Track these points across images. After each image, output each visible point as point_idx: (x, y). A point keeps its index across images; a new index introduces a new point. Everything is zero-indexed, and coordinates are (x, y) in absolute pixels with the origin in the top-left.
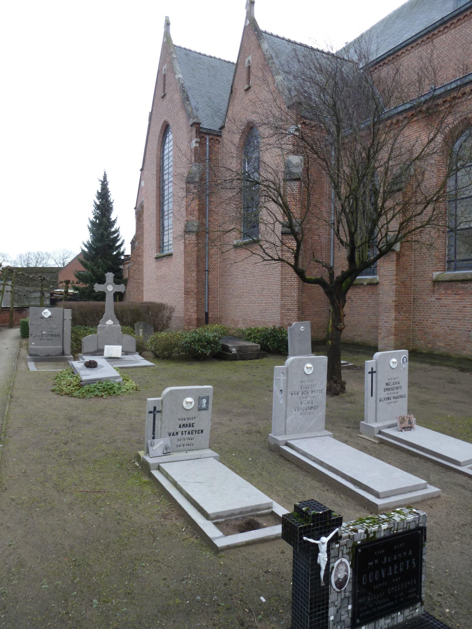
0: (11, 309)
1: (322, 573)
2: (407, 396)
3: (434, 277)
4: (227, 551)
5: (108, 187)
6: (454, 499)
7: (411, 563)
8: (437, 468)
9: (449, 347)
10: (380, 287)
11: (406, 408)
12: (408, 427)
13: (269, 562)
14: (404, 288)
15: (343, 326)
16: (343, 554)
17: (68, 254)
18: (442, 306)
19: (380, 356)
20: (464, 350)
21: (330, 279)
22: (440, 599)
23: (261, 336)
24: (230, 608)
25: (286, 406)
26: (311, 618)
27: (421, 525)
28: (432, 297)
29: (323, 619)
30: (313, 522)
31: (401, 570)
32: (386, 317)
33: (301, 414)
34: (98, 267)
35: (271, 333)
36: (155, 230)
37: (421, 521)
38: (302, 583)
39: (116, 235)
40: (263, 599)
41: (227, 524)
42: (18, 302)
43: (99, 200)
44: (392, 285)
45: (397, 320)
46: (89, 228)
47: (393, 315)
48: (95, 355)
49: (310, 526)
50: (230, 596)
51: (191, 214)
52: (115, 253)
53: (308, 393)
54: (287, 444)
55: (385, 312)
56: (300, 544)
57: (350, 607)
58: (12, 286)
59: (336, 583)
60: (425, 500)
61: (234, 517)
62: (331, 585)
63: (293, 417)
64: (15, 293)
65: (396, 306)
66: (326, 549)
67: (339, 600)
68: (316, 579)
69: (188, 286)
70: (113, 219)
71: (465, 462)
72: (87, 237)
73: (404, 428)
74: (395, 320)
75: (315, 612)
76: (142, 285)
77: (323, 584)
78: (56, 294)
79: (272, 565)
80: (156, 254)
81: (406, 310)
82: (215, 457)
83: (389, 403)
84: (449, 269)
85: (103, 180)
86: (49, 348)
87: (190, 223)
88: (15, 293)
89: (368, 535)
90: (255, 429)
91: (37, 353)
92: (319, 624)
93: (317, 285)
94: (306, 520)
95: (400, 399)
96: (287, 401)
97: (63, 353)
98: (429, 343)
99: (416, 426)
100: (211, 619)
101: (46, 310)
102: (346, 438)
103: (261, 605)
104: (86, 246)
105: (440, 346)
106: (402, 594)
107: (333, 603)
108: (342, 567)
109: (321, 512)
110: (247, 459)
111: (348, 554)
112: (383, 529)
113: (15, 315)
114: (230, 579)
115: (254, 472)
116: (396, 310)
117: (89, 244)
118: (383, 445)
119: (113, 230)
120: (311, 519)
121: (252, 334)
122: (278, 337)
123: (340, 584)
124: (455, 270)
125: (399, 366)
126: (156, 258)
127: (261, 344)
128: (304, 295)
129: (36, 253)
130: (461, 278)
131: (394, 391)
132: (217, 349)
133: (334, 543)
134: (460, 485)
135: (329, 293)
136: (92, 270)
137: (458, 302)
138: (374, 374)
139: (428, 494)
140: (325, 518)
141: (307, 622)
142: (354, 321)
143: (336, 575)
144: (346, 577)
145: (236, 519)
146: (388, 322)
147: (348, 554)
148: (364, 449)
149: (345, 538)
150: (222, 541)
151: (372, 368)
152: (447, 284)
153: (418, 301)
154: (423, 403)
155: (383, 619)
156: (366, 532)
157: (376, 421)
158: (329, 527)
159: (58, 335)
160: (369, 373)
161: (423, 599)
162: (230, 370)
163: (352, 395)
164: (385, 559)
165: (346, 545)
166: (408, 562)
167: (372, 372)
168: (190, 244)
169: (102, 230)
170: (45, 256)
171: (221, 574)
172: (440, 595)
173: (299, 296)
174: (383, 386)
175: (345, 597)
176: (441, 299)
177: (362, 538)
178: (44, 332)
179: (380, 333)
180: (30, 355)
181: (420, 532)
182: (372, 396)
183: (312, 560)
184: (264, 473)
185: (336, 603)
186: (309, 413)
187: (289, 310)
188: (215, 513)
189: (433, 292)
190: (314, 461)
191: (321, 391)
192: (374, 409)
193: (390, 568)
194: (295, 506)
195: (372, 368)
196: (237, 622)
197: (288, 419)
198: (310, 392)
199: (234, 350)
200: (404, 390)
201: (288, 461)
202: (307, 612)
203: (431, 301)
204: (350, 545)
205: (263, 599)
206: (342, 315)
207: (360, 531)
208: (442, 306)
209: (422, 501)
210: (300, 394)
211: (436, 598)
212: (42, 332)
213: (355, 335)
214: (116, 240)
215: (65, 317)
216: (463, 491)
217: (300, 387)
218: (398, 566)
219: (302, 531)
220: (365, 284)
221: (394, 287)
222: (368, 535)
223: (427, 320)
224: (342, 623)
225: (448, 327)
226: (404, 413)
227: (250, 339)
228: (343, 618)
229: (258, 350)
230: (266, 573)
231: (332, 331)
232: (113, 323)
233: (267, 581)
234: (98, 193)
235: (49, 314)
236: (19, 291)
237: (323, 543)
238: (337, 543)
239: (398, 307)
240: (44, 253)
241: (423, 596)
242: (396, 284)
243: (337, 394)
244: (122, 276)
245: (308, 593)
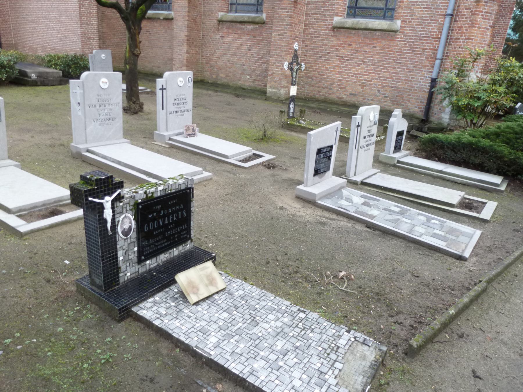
1: (109, 225)
2: (192, 110)
3: (219, 17)
4: (32, 234)
6: (222, 180)
7: (182, 214)
8: (212, 161)
9: (228, 78)
10: (174, 21)
11: (191, 120)
12: (192, 134)
13: (72, 237)
14: (194, 24)
15: (139, 52)
16: (126, 210)
18: (224, 43)
19: (169, 75)
20: (240, 80)
21: (126, 5)
22: (206, 239)
23: (62, 62)
24: (37, 273)
25: (85, 118)
26: (103, 260)
27: (189, 186)
28: (216, 34)
29: (113, 259)
30: (96, 185)
31: (175, 219)
32: (179, 50)
33: (100, 125)
35: (72, 60)
37: (189, 183)
38: (93, 236)
40: (67, 262)
41: (31, 215)
44: (184, 21)
45: (189, 53)
47: (185, 48)
49: (94, 189)
50: (36, 265)
53: (105, 106)
54: (88, 151)
55: (179, 46)
56: (87, 204)
57: (136, 249)
59: (123, 233)
60: (201, 182)
61: (37, 209)
62: (119, 235)
63: (92, 127)
65: (187, 40)
66: (110, 206)
67: (126, 245)
68: (104, 230)
71: (231, 155)
73: (189, 135)
74: (187, 53)
75: (106, 255)
77: (110, 233)
79: (75, 238)
81: (196, 45)
82: (15, 166)
83: (177, 116)
84: (231, 11)
89: (147, 195)
90: (58, 142)
92: (110, 264)
93: (114, 10)
94: (91, 185)
95: (186, 113)
96: (85, 113)
98: (214, 75)
99: (198, 134)
100: (19, 284)
102: (142, 145)
103: (65, 266)
105: (222, 77)
106: (176, 236)
107: (122, 247)
108: (127, 221)
109: (103, 177)
110: (51, 166)
111: (131, 210)
112: (159, 190)
114: (35, 254)
115: (57, 176)
116: (187, 44)
118: (172, 149)
120: (94, 183)
121: (52, 61)
122: (80, 65)
123: (126, 233)
124: (236, 12)
125: (185, 84)
127: (63, 72)
128: (104, 25)
130: (240, 20)
131: (181, 106)
132: (13, 74)
133: (118, 203)
134: (227, 171)
135: (125, 19)
137: (236, 40)
138: (164, 91)
139: (204, 177)
140: (108, 182)
141: (100, 264)
142: (152, 53)
143: (121, 227)
144: (130, 228)
145: (40, 210)
146: (181, 55)
147: (131, 210)
148: (158, 152)
149: (127, 198)
150: (23, 226)
151: (163, 86)
152: (229, 24)
153: (206, 38)
154: (206, 119)
155: (163, 254)
156: (145, 193)
157: (167, 131)
158: (112, 189)
160: (160, 89)
161: (192, 238)
162: (31, 94)
163: (149, 113)
164: (162, 211)
165: (129, 203)
166: (180, 213)
167: (162, 89)
171: (26, 251)
172: (206, 237)
173: (99, 25)
174: (171, 101)
175: (131, 242)
176: (224, 37)
177: (142, 197)
179: (174, 65)
181: (188, 191)
182: (163, 109)
183: (99, 216)
184: (68, 175)
185: (124, 247)
186: (108, 124)
187: (89, 38)
188: (17, 208)
189: (218, 30)
190: (113, 162)
191: (118, 104)
192: (165, 121)
193: (166, 218)
194: (81, 176)
195: (163, 86)
196: (43, 281)
197: (88, 130)
198: (107, 105)
199: (34, 76)
200: (190, 105)
201: (90, 164)
202: (100, 256)
203: (216, 39)
204: (132, 203)
205: (67, 262)
206: (138, 41)
207: (140, 192)
208: (224, 43)
209: (199, 183)
210: (98, 107)
211: (203, 239)
213: (153, 66)
216: (229, 174)
217: (97, 101)
218: (173, 216)
219: (88, 193)
220: (162, 18)
221: (186, 23)
222: (147, 195)
223: (213, 55)
224: (130, 261)
225: (229, 61)
226: (190, 123)
227: (51, 66)
228: (130, 257)
229: (60, 77)
230: (69, 244)
231: (130, 56)
233: (71, 249)
237: (107, 201)
238: (121, 202)
239: (190, 41)
241: (192, 236)
242: (188, 21)
243: (136, 113)
245: (98, 242)
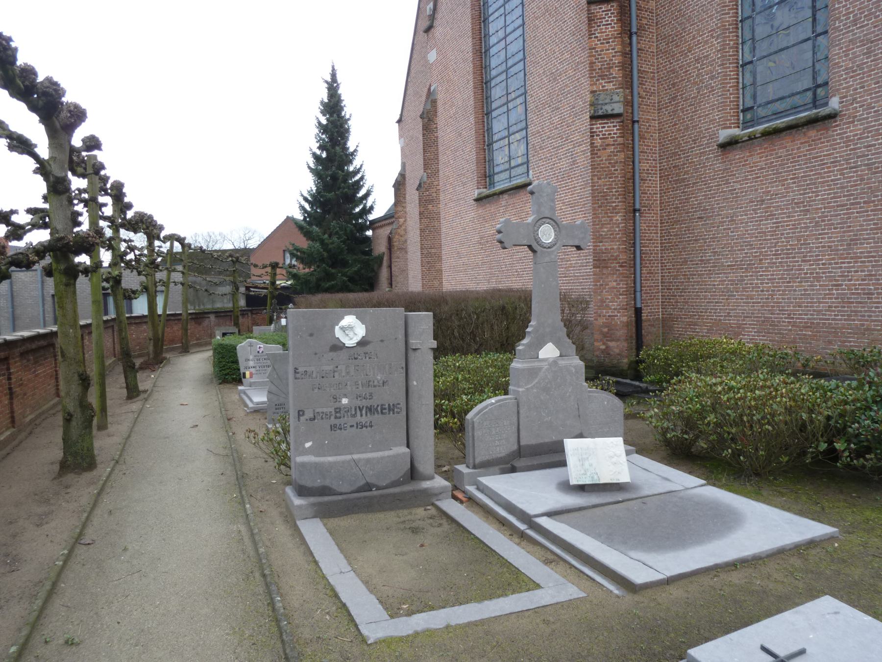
0: (184, 317)
5: (339, 92)
17: (250, 234)
34: (330, 236)
36: (472, 140)
39: (357, 178)
42: (193, 304)
43: (324, 115)
46: (309, 167)
48: (513, 470)
51: (602, 77)
52: (357, 210)
58: (183, 273)
64: (190, 287)
69: (602, 246)
70: (351, 150)
72: (308, 184)
76: (439, 258)
78: (256, 287)
80: (476, 192)
85: (330, 80)
86: (368, 461)
87: (602, 97)
88: (190, 287)
91: (327, 483)
97: (413, 474)
101: (349, 320)
104: (306, 199)
113: (191, 326)
117: (312, 195)
119: (351, 169)
126: (476, 200)
129: (205, 234)
136: (322, 242)
159: (392, 409)
168: (605, 147)
169: (334, 168)
170: (219, 238)
178: (345, 401)
180: (302, 491)
212: (336, 399)
214: (358, 186)
215: (414, 342)
232: (557, 353)
234: (322, 103)
235: (360, 331)
236: (195, 282)
240: (217, 233)
244: (371, 250)
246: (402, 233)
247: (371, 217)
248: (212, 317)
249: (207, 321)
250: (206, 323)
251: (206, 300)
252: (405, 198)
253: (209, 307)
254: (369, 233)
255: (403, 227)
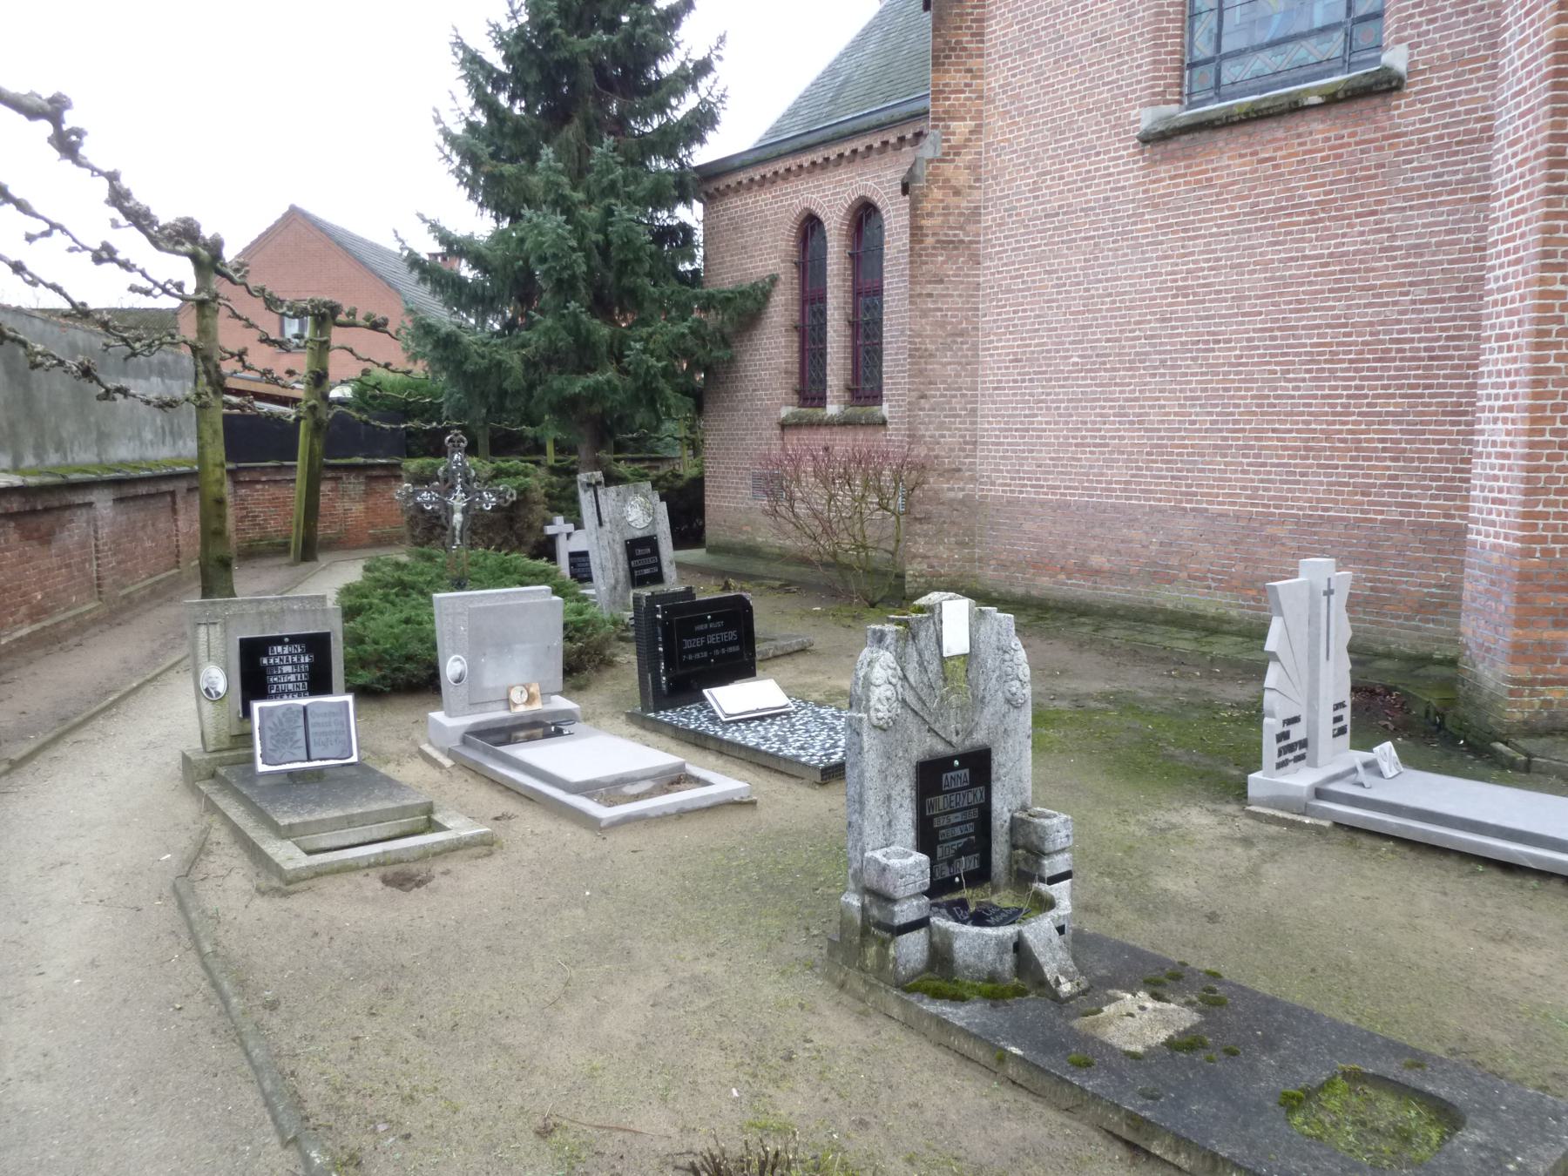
246: (962, 178)
247: (701, 155)
248: (103, 502)
249: (81, 517)
250: (75, 530)
251: (69, 428)
252: (979, 36)
253: (83, 457)
254: (691, 214)
255: (967, 157)
